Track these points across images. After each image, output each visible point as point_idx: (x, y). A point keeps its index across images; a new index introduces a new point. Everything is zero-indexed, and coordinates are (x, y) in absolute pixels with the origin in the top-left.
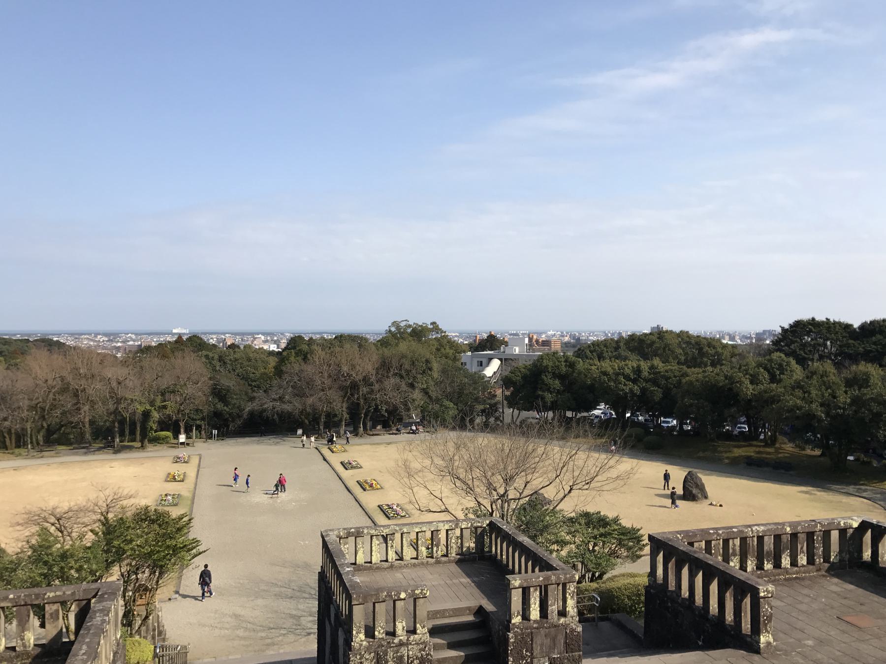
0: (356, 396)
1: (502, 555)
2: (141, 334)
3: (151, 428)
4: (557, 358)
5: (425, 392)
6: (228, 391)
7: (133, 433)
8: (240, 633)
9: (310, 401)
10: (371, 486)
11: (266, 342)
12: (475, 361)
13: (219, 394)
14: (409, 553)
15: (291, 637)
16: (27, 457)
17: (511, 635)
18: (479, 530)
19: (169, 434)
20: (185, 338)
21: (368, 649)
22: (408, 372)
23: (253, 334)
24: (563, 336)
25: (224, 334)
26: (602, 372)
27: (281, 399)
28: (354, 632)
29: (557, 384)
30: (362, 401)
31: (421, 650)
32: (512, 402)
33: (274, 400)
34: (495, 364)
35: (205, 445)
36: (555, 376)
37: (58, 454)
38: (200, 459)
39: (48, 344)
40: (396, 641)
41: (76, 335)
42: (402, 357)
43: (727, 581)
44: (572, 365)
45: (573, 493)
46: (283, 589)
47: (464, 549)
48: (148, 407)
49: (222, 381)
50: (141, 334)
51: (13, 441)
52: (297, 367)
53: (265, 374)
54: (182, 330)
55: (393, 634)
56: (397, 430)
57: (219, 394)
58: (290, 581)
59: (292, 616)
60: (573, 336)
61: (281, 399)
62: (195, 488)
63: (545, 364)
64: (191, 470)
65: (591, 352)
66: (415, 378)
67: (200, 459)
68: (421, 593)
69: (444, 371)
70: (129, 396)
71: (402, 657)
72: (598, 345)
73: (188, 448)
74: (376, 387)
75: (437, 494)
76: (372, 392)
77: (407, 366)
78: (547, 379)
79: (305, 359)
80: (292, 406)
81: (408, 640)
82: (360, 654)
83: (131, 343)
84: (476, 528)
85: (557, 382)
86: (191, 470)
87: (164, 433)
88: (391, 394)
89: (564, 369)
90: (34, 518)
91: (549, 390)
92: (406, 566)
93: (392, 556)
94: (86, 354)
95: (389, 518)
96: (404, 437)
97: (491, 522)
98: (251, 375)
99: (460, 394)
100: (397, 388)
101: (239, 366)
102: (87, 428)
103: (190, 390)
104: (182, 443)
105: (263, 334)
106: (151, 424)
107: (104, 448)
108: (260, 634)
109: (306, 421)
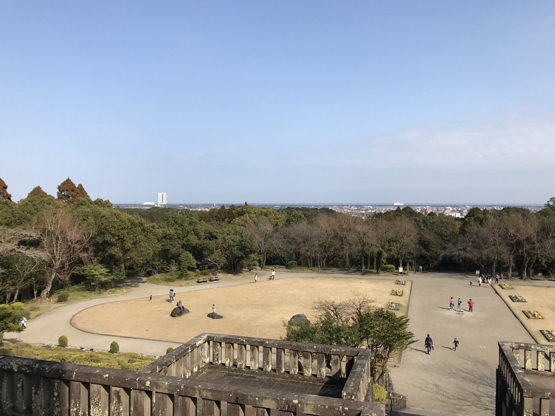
0: (521, 251)
2: (375, 206)
3: (383, 262)
6: (429, 242)
7: (372, 264)
8: (439, 397)
10: (534, 315)
11: (453, 211)
13: (423, 244)
16: (318, 272)
19: (393, 266)
25: (426, 206)
27: (464, 249)
37: (333, 272)
39: (327, 211)
41: (341, 206)
46: (468, 375)
48: (381, 249)
49: (425, 236)
50: (375, 206)
52: (475, 229)
53: (453, 232)
57: (423, 244)
58: (472, 370)
59: (475, 395)
61: (464, 249)
64: (406, 290)
73: (405, 276)
79: (481, 223)
80: (473, 255)
83: (370, 211)
86: (406, 290)
87: (390, 265)
90: (324, 306)
98: (444, 233)
103: (405, 240)
104: (401, 273)
105: (451, 206)
106: (382, 259)
107: (357, 271)
108: (452, 401)
109: (482, 265)
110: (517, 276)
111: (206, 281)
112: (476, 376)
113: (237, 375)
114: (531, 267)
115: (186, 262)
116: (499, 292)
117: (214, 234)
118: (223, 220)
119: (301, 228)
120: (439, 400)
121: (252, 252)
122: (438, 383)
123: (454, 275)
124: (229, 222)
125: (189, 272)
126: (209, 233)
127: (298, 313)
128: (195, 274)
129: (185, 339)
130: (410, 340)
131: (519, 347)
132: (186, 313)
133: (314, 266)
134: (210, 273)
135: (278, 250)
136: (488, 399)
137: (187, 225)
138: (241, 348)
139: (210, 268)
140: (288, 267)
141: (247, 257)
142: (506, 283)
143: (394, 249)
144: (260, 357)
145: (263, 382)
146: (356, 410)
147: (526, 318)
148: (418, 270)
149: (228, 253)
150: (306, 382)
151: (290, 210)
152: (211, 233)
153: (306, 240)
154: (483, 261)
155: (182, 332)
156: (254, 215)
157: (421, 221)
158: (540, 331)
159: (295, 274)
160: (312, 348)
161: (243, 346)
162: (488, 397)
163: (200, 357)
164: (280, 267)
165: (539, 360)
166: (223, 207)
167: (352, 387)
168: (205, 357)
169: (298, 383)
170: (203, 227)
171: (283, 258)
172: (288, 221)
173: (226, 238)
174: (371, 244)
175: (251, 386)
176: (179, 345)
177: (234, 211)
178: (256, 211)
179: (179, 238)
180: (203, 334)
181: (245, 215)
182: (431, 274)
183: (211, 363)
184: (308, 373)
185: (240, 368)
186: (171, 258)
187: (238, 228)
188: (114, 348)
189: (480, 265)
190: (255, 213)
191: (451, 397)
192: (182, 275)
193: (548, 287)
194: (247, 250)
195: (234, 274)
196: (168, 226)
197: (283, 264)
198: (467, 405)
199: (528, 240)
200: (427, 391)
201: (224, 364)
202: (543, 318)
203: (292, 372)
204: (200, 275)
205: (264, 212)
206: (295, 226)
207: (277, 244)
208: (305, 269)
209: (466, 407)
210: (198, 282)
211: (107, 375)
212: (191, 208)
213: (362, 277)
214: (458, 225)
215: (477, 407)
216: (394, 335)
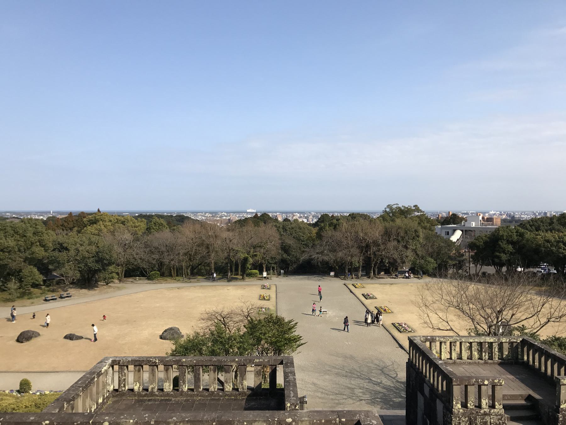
0: (369, 253)
1: (534, 362)
2: (229, 213)
3: (248, 268)
4: (510, 230)
5: (415, 251)
6: (290, 247)
7: (237, 270)
8: (319, 394)
10: (385, 310)
11: (300, 217)
12: (444, 231)
13: (285, 249)
14: (465, 355)
15: (351, 401)
16: (183, 282)
17: (560, 416)
18: (515, 345)
19: (257, 271)
20: (259, 215)
21: (464, 414)
22: (403, 238)
23: (292, 213)
24: (502, 215)
25: (276, 212)
26: (545, 240)
27: (322, 253)
28: (454, 403)
29: (510, 248)
30: (372, 256)
31: (499, 419)
32: (476, 259)
33: (318, 253)
34: (458, 234)
35: (277, 279)
36: (509, 242)
37: (198, 281)
39: (181, 219)
40: (482, 411)
41: (195, 213)
42: (399, 228)
43: (493, 397)
44: (521, 235)
45: (549, 324)
46: (339, 370)
47: (504, 356)
48: (247, 256)
49: (286, 241)
50: (229, 213)
52: (330, 233)
53: (310, 237)
54: (251, 210)
55: (479, 406)
56: (396, 275)
58: (343, 366)
59: (349, 388)
60: (509, 215)
61: (322, 253)
63: (501, 234)
64: (272, 293)
65: (531, 226)
66: (407, 242)
68: (499, 382)
69: (427, 238)
70: (235, 247)
71: (486, 422)
72: (536, 221)
74: (382, 247)
75: (444, 318)
78: (503, 244)
79: (335, 228)
80: (329, 257)
81: (490, 411)
82: (459, 417)
83: (224, 218)
84: (512, 343)
85: (510, 246)
86: (272, 293)
87: (254, 271)
88: (392, 252)
89: (516, 238)
90: (210, 317)
91: (504, 252)
92: (464, 363)
93: (454, 356)
94: (202, 224)
96: (400, 280)
97: (523, 340)
99: (438, 253)
100: (396, 248)
101: (294, 232)
102: (213, 266)
103: (269, 246)
104: (265, 278)
105: (298, 213)
106: (248, 265)
108: (331, 397)
109: (337, 267)
110: (365, 276)
111: (56, 299)
113: (149, 400)
115: (30, 278)
116: (353, 291)
117: (65, 245)
118: (71, 229)
119: (165, 236)
120: (320, 398)
121: (110, 264)
122: (316, 381)
123: (312, 277)
124: (79, 232)
125: (32, 290)
126: (59, 244)
127: (170, 327)
128: (40, 291)
129: (88, 365)
130: (298, 342)
131: (427, 340)
132: (36, 337)
133: (177, 276)
134: (59, 289)
135: (139, 261)
136: (361, 391)
137: (31, 235)
138: (153, 370)
139: (58, 283)
140: (150, 278)
141: (104, 270)
142: (358, 283)
143: (260, 254)
144: (146, 376)
145: (181, 403)
146: (353, 420)
148: (279, 274)
149: (82, 265)
150: (227, 397)
151: (147, 217)
152: (61, 245)
153: (170, 249)
154: (337, 263)
155: (82, 358)
156: (110, 224)
159: (159, 286)
160: (234, 361)
161: (155, 367)
162: (360, 389)
163: (105, 384)
164: (140, 279)
165: (442, 350)
166: (71, 214)
167: (293, 397)
168: (109, 385)
169: (219, 400)
170: (51, 237)
171: (144, 268)
172: (148, 229)
173: (80, 249)
174: (238, 251)
175: (169, 410)
176: (81, 375)
177: (85, 219)
178: (112, 219)
179: (19, 250)
180: (107, 358)
181: (98, 224)
183: (116, 390)
184: (229, 388)
185: (152, 391)
186: (9, 274)
187: (94, 239)
188: (24, 387)
189: (335, 267)
190: (111, 221)
191: (329, 393)
192: (25, 293)
193: (392, 284)
194: (105, 261)
195: (89, 289)
196: (6, 237)
198: (344, 399)
199: (376, 243)
200: (307, 391)
201: (132, 390)
203: (212, 389)
204: (47, 292)
205: (121, 220)
206: (157, 235)
207: (138, 254)
208: (169, 279)
209: (344, 401)
210: (46, 300)
211: (47, 422)
212: (21, 216)
213: (227, 283)
214: (315, 230)
215: (353, 399)
216: (285, 339)
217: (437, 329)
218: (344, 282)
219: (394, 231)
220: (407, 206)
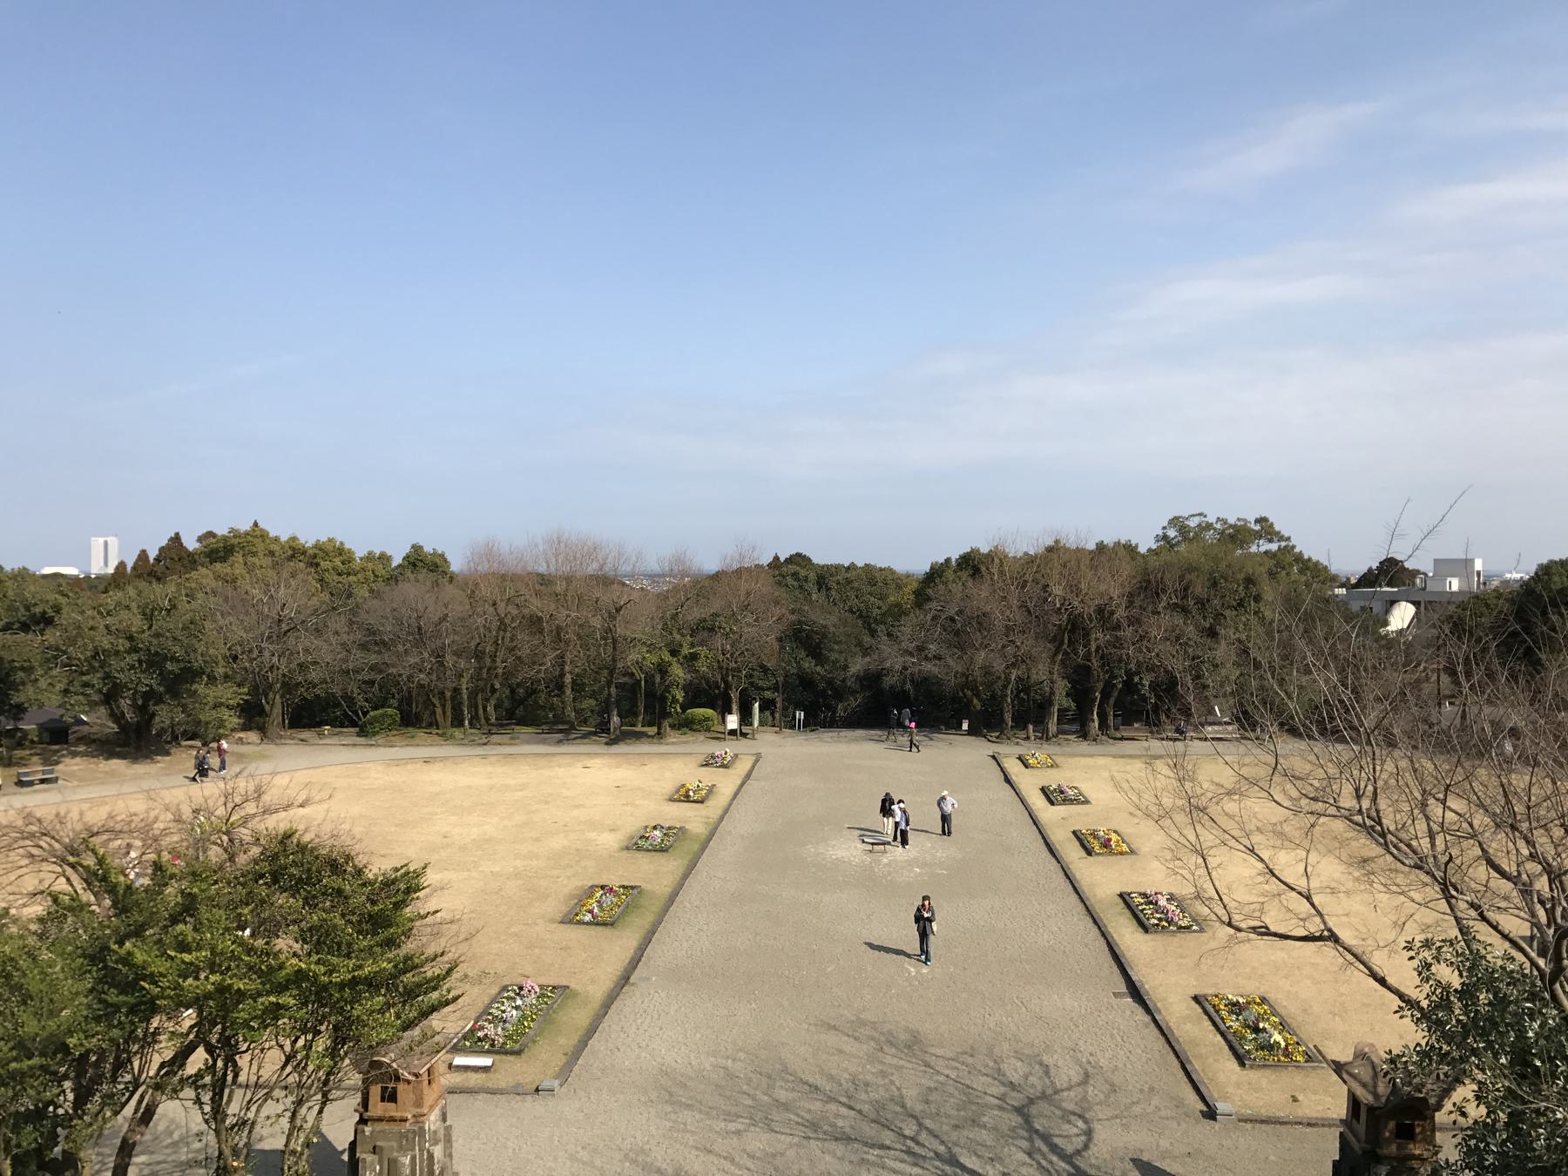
6: (824, 636)
9: (981, 656)
10: (1106, 844)
22: (1202, 603)
30: (1095, 663)
37: (514, 740)
38: (757, 761)
51: (449, 713)
56: (1179, 731)
57: (805, 639)
62: (722, 818)
66: (1219, 616)
67: (757, 761)
73: (744, 741)
74: (1127, 633)
75: (1293, 875)
76: (1117, 643)
77: (1199, 589)
80: (945, 668)
86: (726, 782)
87: (701, 710)
95: (1146, 930)
98: (876, 611)
104: (733, 732)
107: (595, 733)
112: (866, 1108)
114: (1112, 700)
116: (1014, 778)
140: (363, 732)
142: (1039, 752)
147: (1084, 854)
156: (268, 561)
157: (812, 576)
158: (1121, 895)
182: (828, 735)
190: (272, 553)
194: (169, 666)
197: (354, 724)
202: (1132, 852)
208: (421, 734)
217: (1254, 929)
218: (993, 748)
219: (1171, 582)
220: (1232, 521)
